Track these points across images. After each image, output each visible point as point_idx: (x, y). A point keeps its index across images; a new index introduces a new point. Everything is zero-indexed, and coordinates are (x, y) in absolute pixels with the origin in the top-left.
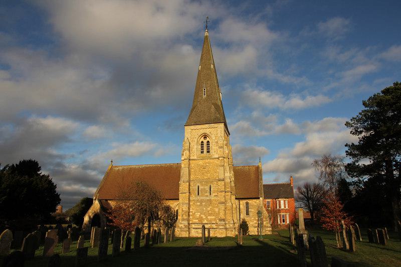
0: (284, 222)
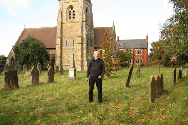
0: (139, 54)
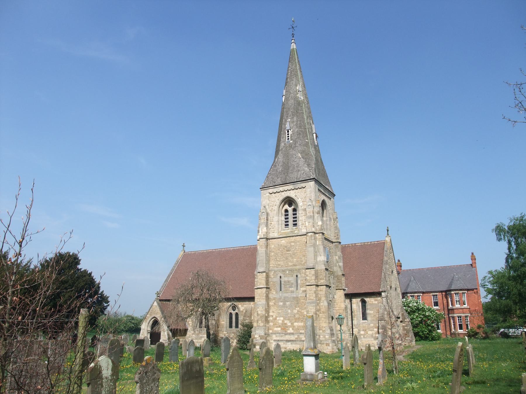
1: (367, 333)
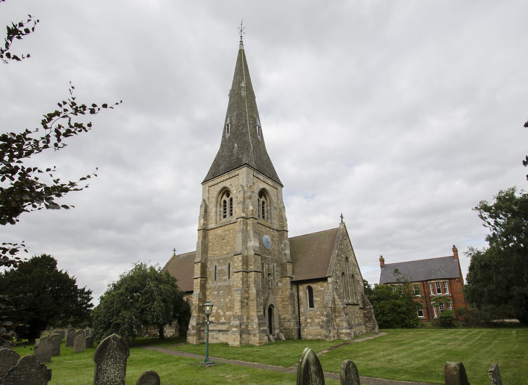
0: (439, 291)
1: (314, 322)
